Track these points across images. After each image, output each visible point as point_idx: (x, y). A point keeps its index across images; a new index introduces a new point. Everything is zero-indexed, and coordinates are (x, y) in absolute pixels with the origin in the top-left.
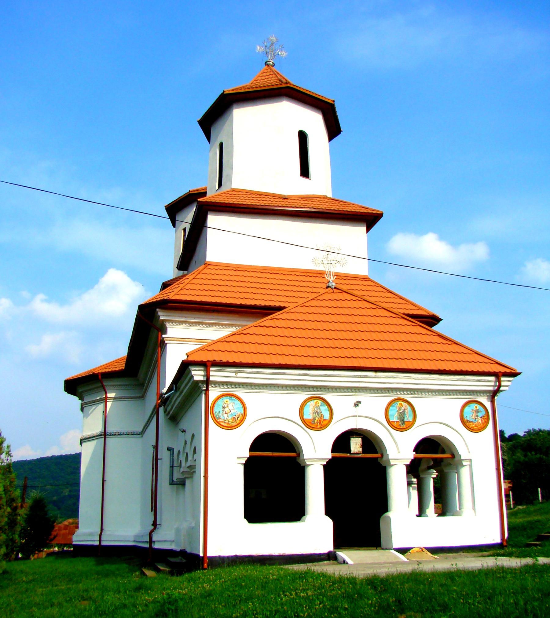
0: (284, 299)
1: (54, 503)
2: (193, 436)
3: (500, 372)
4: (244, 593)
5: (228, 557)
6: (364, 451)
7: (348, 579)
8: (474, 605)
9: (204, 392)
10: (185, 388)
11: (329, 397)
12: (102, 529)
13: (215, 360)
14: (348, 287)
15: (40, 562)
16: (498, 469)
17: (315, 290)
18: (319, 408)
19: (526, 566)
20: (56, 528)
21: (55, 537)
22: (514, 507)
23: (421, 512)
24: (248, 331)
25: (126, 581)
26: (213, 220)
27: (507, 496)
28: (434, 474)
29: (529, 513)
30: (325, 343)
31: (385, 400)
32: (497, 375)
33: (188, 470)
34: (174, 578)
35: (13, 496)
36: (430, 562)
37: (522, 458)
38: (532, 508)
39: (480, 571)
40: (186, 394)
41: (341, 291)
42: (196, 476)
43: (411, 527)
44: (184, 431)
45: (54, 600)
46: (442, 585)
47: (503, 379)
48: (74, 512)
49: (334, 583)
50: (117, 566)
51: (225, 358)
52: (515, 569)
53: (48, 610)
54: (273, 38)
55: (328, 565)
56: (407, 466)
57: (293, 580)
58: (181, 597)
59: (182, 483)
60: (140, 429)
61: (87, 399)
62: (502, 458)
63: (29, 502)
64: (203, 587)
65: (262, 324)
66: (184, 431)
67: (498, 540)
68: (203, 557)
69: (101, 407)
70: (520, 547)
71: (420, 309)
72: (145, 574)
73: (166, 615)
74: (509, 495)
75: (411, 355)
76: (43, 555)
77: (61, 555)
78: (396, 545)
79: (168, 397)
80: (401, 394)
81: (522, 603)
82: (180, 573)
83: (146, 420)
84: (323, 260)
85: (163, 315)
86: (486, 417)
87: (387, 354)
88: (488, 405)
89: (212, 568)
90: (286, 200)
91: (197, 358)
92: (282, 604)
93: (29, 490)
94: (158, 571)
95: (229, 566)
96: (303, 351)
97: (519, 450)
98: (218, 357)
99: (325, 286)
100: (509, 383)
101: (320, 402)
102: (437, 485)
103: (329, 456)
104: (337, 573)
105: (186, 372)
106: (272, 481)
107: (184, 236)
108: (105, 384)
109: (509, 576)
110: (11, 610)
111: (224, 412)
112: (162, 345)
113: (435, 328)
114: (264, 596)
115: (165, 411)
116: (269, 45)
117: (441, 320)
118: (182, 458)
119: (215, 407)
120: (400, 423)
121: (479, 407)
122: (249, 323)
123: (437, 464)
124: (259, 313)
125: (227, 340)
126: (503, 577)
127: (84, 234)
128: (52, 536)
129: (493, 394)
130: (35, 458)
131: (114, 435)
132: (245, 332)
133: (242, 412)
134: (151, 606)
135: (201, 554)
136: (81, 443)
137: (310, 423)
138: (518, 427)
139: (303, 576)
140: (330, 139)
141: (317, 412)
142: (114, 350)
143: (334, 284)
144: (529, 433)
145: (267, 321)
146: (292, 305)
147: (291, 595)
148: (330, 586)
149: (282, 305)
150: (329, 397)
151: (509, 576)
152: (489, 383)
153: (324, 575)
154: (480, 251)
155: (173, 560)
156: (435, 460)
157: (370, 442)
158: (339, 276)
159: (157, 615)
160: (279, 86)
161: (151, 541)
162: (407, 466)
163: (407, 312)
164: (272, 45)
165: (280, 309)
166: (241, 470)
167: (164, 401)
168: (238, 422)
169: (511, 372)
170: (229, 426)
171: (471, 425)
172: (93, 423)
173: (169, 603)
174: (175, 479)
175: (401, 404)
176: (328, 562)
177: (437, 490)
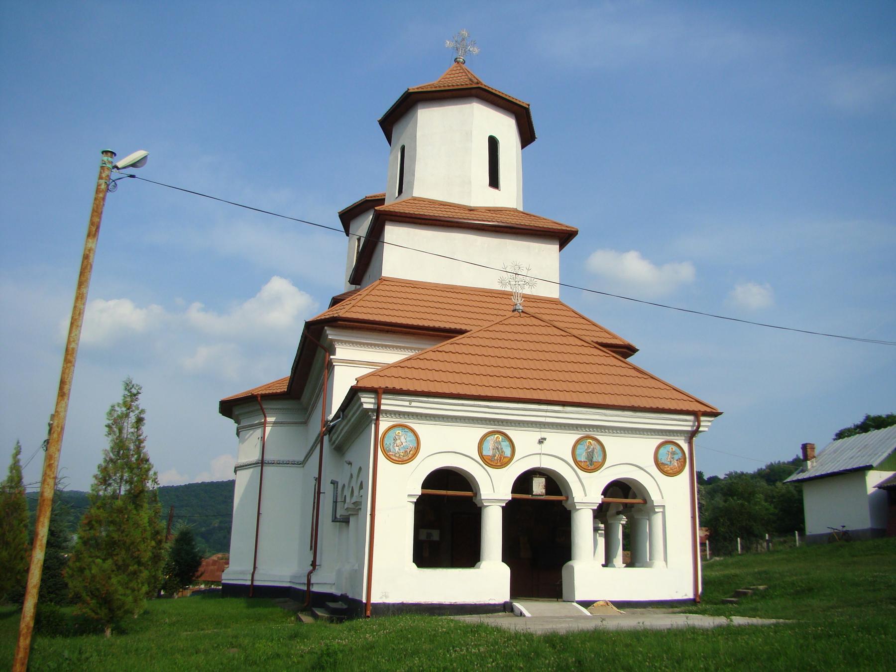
0: (465, 321)
1: (203, 535)
2: (360, 469)
4: (410, 646)
5: (394, 605)
6: (547, 493)
7: (524, 635)
8: (660, 669)
9: (374, 422)
10: (353, 415)
11: (511, 432)
12: (255, 568)
14: (537, 310)
15: (184, 601)
16: (693, 518)
17: (500, 312)
19: (720, 627)
20: (204, 563)
21: (201, 575)
22: (711, 558)
23: (608, 562)
24: (425, 356)
25: (279, 626)
26: (392, 233)
27: (703, 544)
28: (624, 520)
29: (727, 566)
30: (510, 336)
31: (572, 438)
32: (696, 414)
33: (351, 506)
34: (333, 625)
35: (158, 528)
36: (615, 617)
37: (722, 504)
38: (730, 560)
39: (669, 630)
40: (355, 421)
42: (361, 513)
43: (595, 577)
44: (350, 463)
45: (199, 646)
46: (627, 646)
47: (702, 418)
48: (224, 546)
49: (509, 639)
50: (270, 609)
52: (707, 630)
53: (193, 658)
54: (465, 33)
55: (503, 617)
56: (593, 510)
57: (465, 633)
58: (341, 648)
59: (346, 521)
60: (302, 459)
61: (244, 423)
62: (699, 503)
63: (175, 534)
64: (365, 638)
65: (440, 349)
66: (350, 463)
67: (691, 596)
68: (366, 604)
69: (258, 432)
70: (716, 604)
71: (615, 337)
72: (300, 620)
73: (322, 668)
74: (705, 544)
76: (188, 593)
77: (209, 594)
78: (578, 597)
79: (334, 426)
81: (713, 668)
82: (341, 621)
83: (307, 451)
85: (331, 334)
87: (577, 387)
91: (368, 384)
92: (451, 661)
93: (174, 519)
94: (315, 617)
95: (394, 614)
97: (720, 495)
99: (512, 308)
100: (709, 424)
102: (627, 531)
103: (509, 497)
104: (512, 627)
105: (355, 398)
106: (446, 524)
107: (359, 246)
108: (264, 407)
109: (701, 637)
110: (151, 656)
112: (330, 367)
113: (629, 360)
114: (432, 650)
115: (330, 441)
116: (459, 40)
118: (347, 493)
119: (386, 439)
121: (675, 448)
122: (428, 347)
123: (627, 509)
124: (438, 336)
125: (402, 365)
126: (693, 639)
127: (247, 238)
128: (199, 573)
129: (691, 435)
130: (183, 484)
131: (272, 463)
132: (421, 357)
133: (415, 445)
134: (307, 658)
135: (364, 601)
136: (235, 472)
138: (719, 469)
139: (476, 629)
140: (523, 147)
142: (277, 370)
143: (521, 307)
144: (730, 476)
145: (446, 345)
146: (475, 329)
147: (462, 650)
148: (505, 642)
149: (464, 327)
150: (511, 432)
151: (701, 637)
152: (685, 423)
153: (498, 630)
154: (686, 272)
155: (332, 605)
156: (625, 505)
157: (555, 484)
158: (527, 298)
159: (313, 668)
160: (469, 86)
161: (309, 584)
162: (593, 510)
163: (600, 340)
164: (463, 40)
165: (461, 332)
166: (411, 508)
167: (329, 430)
171: (667, 469)
172: (250, 451)
173: (328, 655)
174: (338, 516)
176: (503, 613)
177: (626, 536)
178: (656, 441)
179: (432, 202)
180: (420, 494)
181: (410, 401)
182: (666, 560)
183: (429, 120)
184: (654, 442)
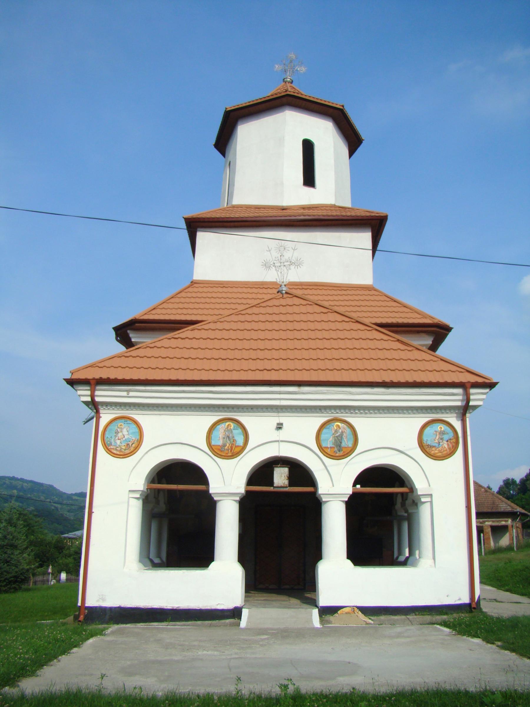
3: (469, 382)
5: (111, 609)
6: (291, 484)
11: (246, 419)
13: (101, 378)
16: (468, 507)
18: (232, 432)
41: (291, 296)
47: (472, 391)
51: (113, 374)
54: (292, 56)
67: (466, 600)
71: (425, 316)
75: (352, 364)
80: (337, 413)
84: (275, 262)
86: (454, 440)
88: (457, 425)
89: (86, 623)
90: (284, 211)
96: (221, 365)
98: (104, 374)
100: (484, 397)
101: (232, 425)
111: (117, 438)
117: (451, 328)
119: (107, 433)
120: (336, 449)
121: (443, 427)
129: (465, 410)
133: (138, 437)
137: (219, 449)
141: (228, 437)
150: (246, 419)
152: (454, 398)
157: (300, 473)
164: (291, 62)
168: (132, 449)
169: (484, 383)
170: (122, 454)
171: (434, 451)
175: (338, 426)
178: (421, 420)
179: (248, 207)
180: (351, 492)
181: (128, 391)
182: (434, 558)
183: (246, 132)
184: (418, 421)
